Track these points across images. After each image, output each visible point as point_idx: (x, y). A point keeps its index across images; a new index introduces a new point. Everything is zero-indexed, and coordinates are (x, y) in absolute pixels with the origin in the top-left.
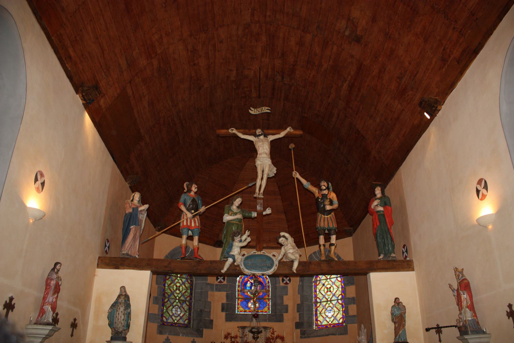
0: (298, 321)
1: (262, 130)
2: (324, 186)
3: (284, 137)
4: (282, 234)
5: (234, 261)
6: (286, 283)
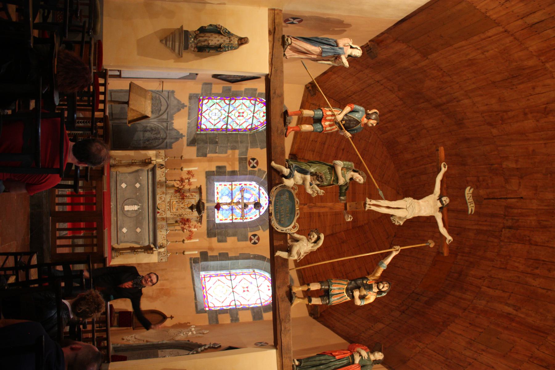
0: (209, 255)
2: (383, 287)
3: (440, 232)
4: (322, 236)
5: (287, 177)
6: (251, 240)
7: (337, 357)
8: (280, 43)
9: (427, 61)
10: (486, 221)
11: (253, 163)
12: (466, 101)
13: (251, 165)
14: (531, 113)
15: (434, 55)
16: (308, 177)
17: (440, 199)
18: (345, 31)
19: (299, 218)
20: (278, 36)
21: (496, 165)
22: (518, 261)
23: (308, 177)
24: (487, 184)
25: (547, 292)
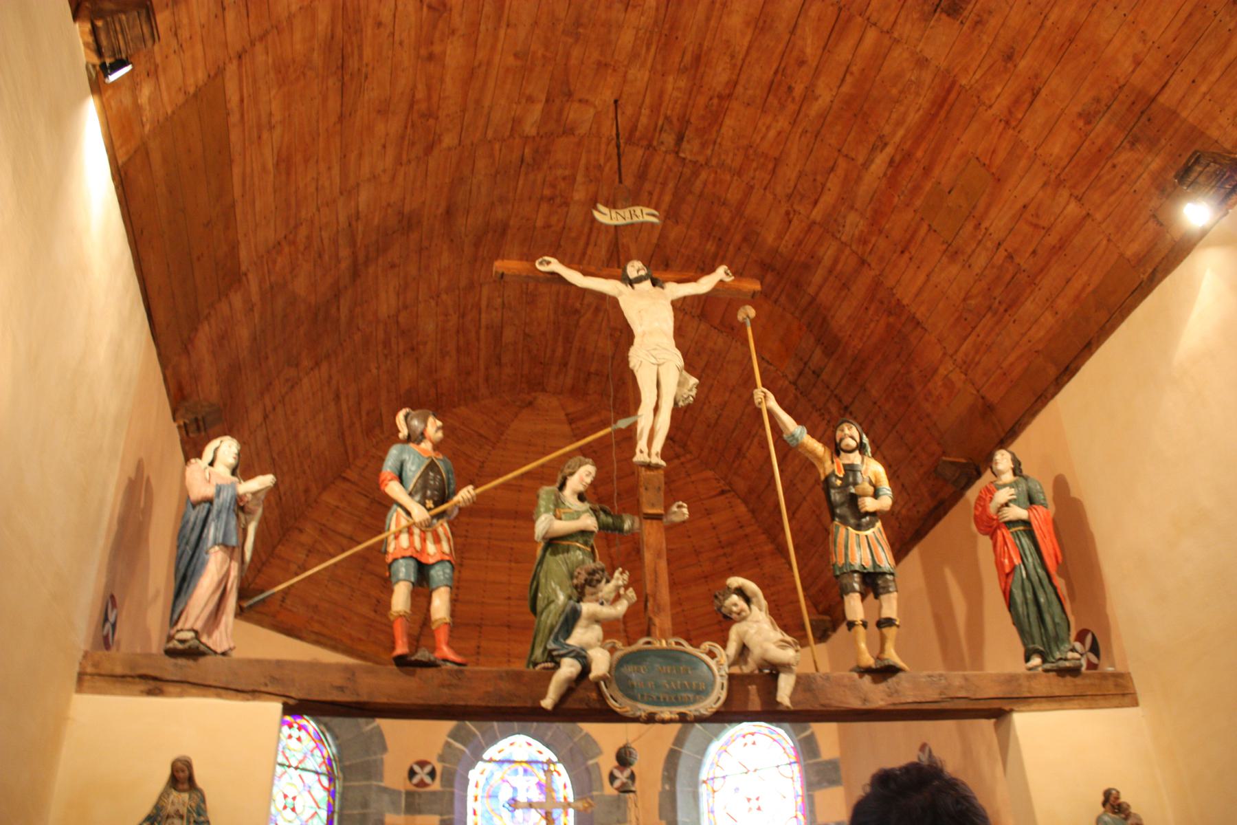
1: (647, 264)
2: (852, 438)
4: (735, 581)
5: (586, 669)
7: (1017, 561)
8: (190, 663)
9: (250, 276)
10: (650, 193)
11: (422, 774)
12: (364, 196)
13: (428, 780)
14: (432, 43)
15: (243, 254)
16: (587, 607)
17: (631, 283)
18: (148, 480)
19: (689, 640)
20: (171, 668)
21: (527, 150)
22: (764, 129)
23: (587, 607)
24: (564, 179)
25: (852, 74)
